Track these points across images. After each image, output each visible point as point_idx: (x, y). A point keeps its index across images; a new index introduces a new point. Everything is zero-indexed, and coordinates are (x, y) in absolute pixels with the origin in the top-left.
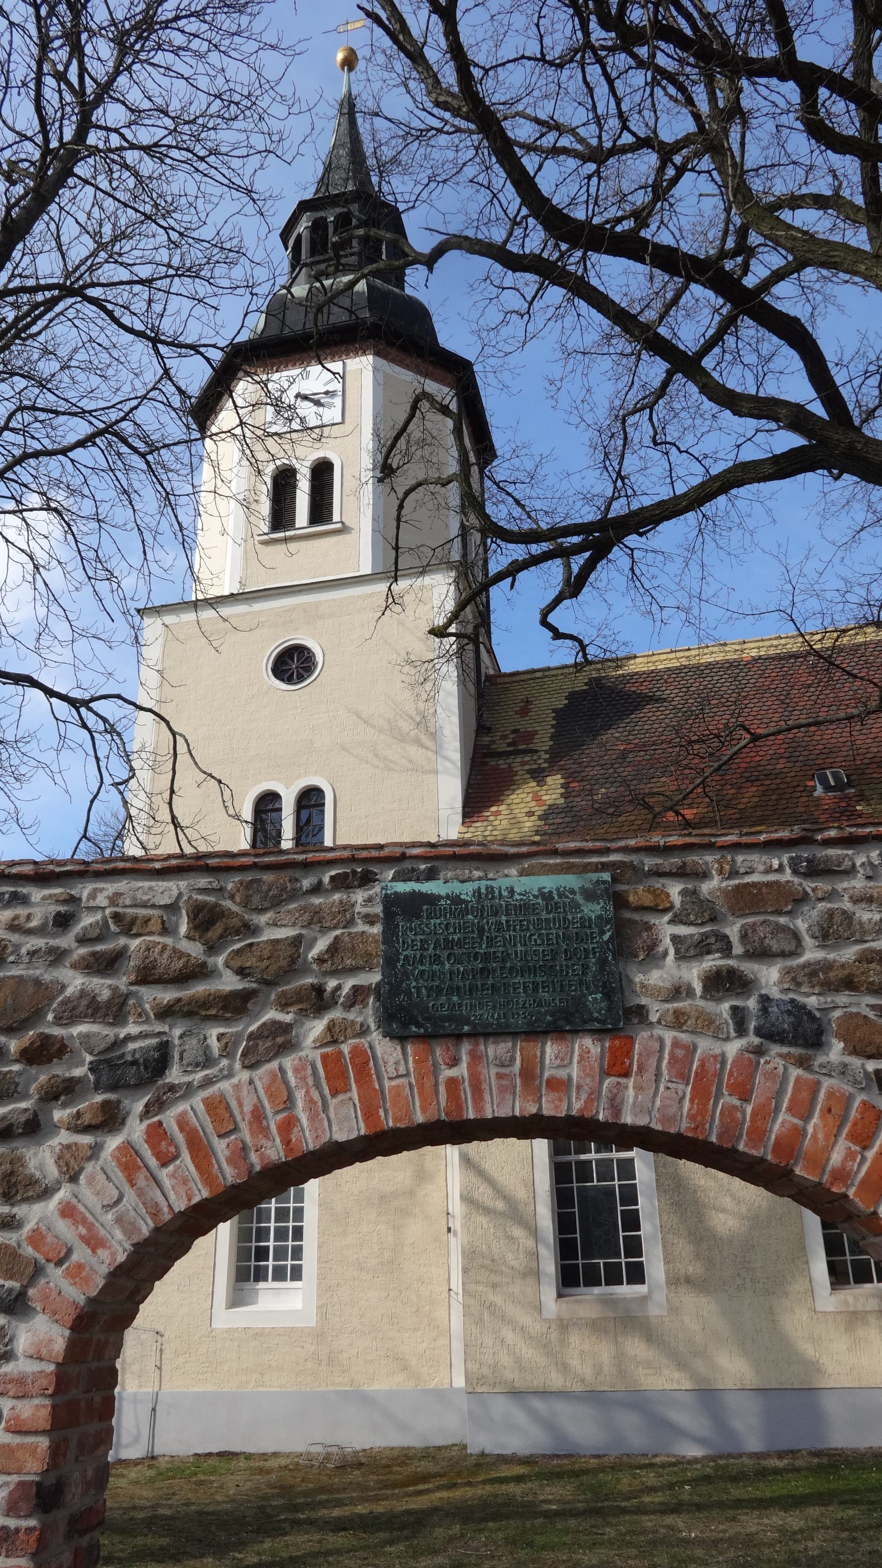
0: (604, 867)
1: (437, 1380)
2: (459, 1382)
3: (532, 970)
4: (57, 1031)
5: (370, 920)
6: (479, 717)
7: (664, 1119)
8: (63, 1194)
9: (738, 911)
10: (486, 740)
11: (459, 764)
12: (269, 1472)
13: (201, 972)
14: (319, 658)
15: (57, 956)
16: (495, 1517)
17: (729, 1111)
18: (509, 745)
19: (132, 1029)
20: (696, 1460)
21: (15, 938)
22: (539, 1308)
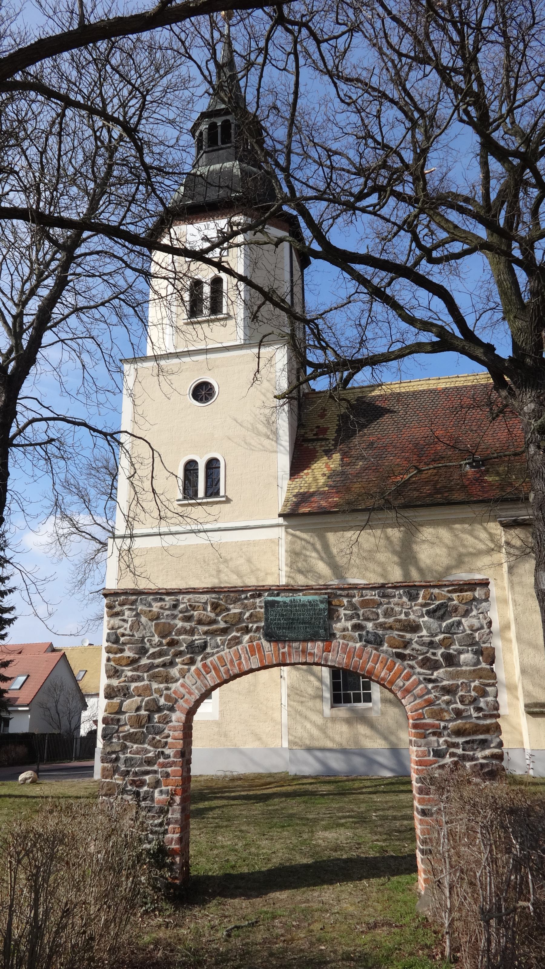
0: (326, 593)
1: (275, 744)
2: (286, 745)
3: (306, 623)
4: (176, 637)
5: (261, 607)
6: (299, 419)
7: (339, 663)
8: (181, 681)
9: (363, 607)
10: (303, 431)
11: (288, 448)
12: (200, 781)
13: (214, 622)
14: (216, 389)
15: (174, 617)
16: (299, 796)
17: (356, 661)
18: (314, 435)
19: (196, 637)
20: (390, 778)
21: (162, 611)
22: (322, 712)
